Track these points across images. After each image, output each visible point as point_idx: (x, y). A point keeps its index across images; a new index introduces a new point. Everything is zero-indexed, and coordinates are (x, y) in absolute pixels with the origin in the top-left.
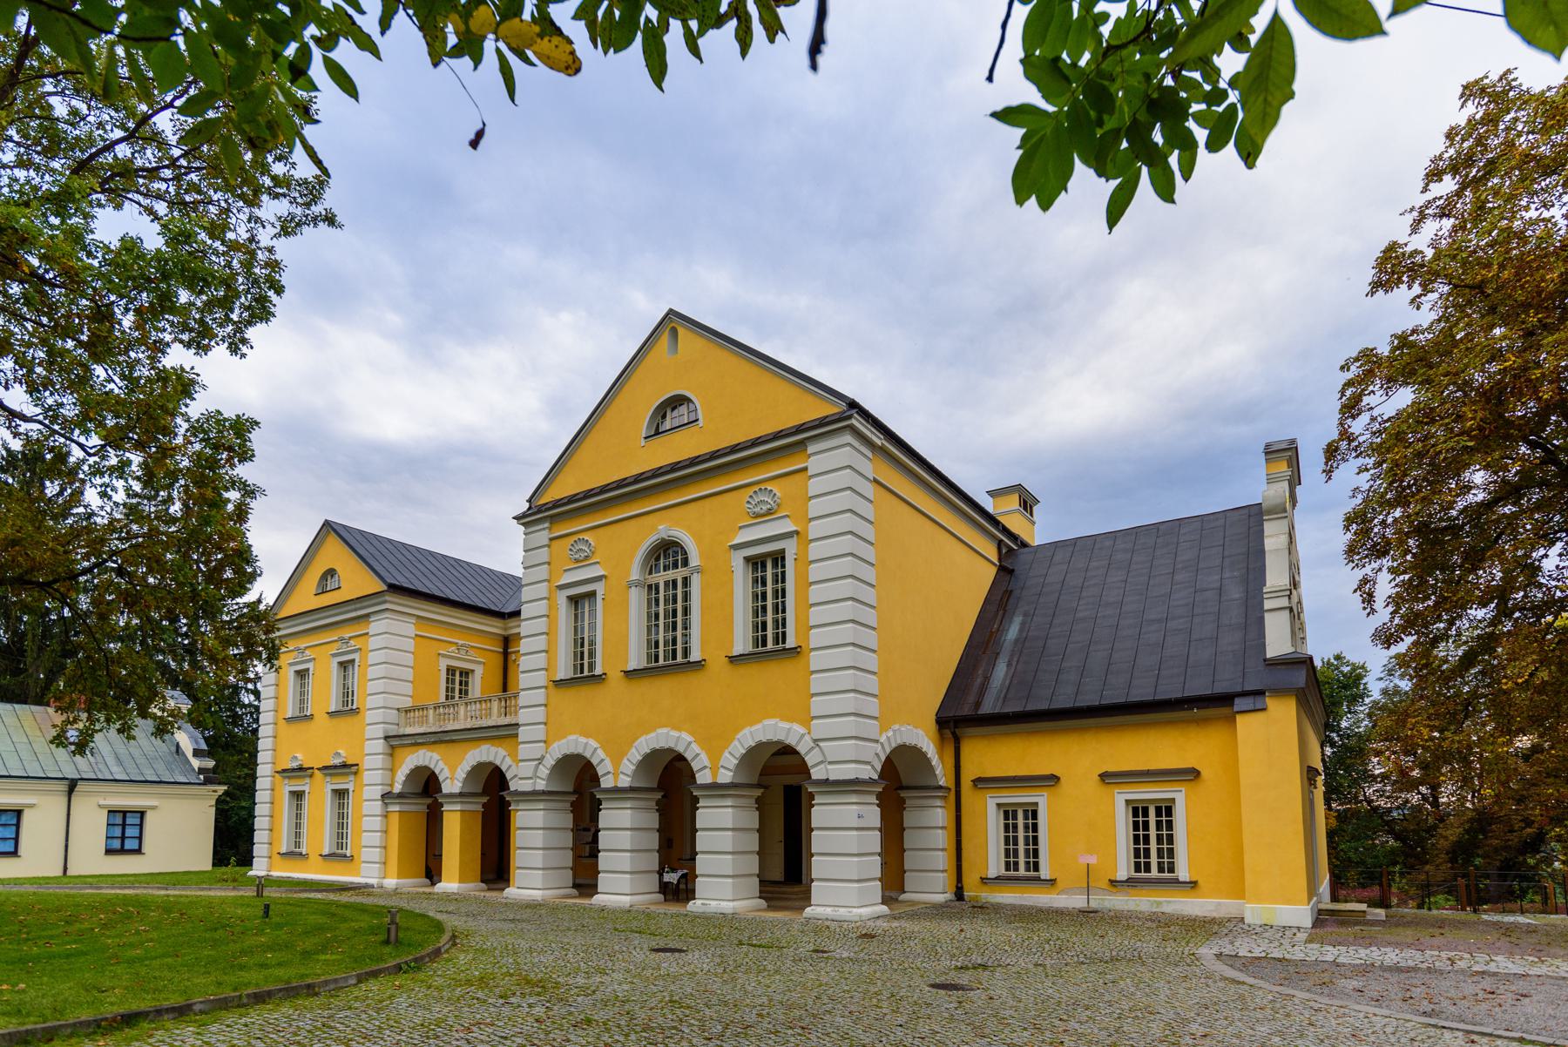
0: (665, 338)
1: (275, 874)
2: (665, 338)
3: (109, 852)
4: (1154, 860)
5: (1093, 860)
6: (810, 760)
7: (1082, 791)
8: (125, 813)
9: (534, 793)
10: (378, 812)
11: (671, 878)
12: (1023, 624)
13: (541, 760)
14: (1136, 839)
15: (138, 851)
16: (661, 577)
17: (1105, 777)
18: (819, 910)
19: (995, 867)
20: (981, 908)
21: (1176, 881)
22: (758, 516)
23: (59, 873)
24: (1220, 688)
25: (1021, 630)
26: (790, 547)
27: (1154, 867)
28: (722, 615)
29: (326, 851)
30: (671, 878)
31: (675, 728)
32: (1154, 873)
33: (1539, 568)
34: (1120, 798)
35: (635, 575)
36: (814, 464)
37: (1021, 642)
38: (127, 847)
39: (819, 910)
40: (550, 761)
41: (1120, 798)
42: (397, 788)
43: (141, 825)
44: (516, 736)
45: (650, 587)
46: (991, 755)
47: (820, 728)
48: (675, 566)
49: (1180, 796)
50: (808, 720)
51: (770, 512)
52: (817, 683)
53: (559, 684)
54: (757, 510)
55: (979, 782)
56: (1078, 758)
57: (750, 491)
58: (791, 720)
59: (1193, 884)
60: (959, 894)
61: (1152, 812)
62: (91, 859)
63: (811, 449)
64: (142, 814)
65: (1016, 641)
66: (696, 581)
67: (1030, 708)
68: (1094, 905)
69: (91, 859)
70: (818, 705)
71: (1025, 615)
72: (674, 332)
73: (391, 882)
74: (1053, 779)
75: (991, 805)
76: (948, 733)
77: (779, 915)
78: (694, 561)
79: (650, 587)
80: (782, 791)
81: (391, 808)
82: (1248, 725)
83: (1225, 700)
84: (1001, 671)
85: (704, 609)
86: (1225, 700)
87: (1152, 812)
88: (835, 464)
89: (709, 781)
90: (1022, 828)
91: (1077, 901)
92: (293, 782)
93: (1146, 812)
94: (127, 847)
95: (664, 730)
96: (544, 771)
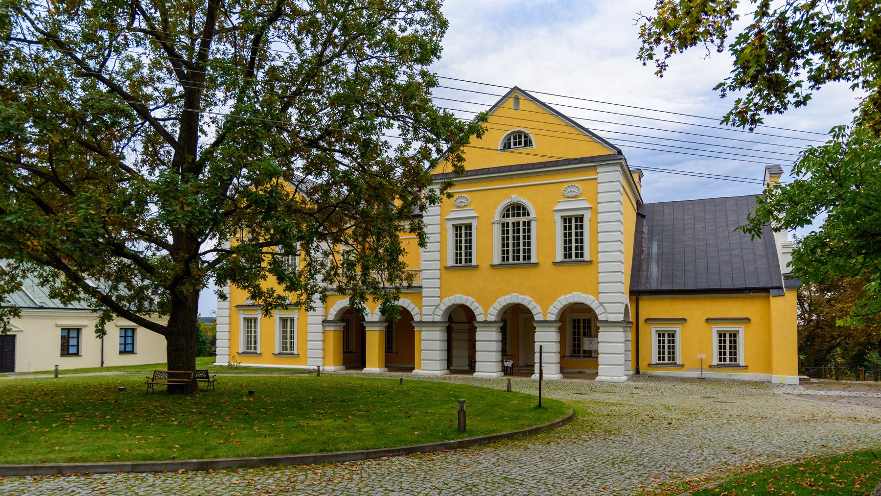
0: (510, 102)
1: (242, 365)
2: (510, 102)
3: (121, 353)
4: (728, 357)
5: (704, 356)
6: (597, 311)
7: (697, 327)
8: (69, 329)
9: (433, 322)
10: (227, 330)
11: (509, 364)
12: (659, 245)
13: (437, 306)
14: (735, 348)
15: (77, 354)
16: (510, 220)
17: (708, 320)
18: (603, 378)
19: (655, 360)
20: (652, 378)
21: (739, 366)
22: (569, 197)
23: (99, 365)
24: (762, 284)
25: (659, 248)
26: (587, 216)
27: (728, 359)
28: (547, 242)
29: (277, 352)
30: (509, 364)
31: (521, 293)
32: (728, 362)
33: (743, 64)
34: (715, 329)
35: (497, 217)
36: (601, 177)
37: (660, 255)
38: (71, 352)
39: (603, 378)
40: (443, 307)
41: (715, 329)
42: (331, 317)
43: (78, 338)
44: (421, 293)
45: (503, 224)
46: (651, 308)
47: (603, 298)
48: (519, 215)
49: (741, 329)
50: (597, 294)
51: (576, 196)
52: (602, 277)
53: (447, 268)
54: (570, 194)
55: (648, 320)
56: (695, 311)
57: (566, 185)
58: (587, 293)
59: (746, 367)
60: (637, 371)
61: (728, 336)
62: (114, 358)
63: (599, 170)
64: (78, 330)
65: (658, 254)
66: (534, 226)
67: (675, 288)
68: (704, 376)
69: (114, 358)
70: (602, 287)
71: (659, 241)
72: (517, 99)
73: (330, 368)
74: (684, 320)
75: (653, 331)
76: (634, 297)
77: (568, 381)
78: (533, 215)
79: (503, 224)
80: (579, 326)
81: (327, 329)
82: (775, 302)
83: (765, 290)
84: (654, 269)
85: (538, 239)
86: (765, 290)
87: (728, 336)
88: (609, 179)
89: (542, 319)
90: (666, 343)
91: (696, 374)
92: (247, 312)
93: (725, 336)
94: (71, 352)
95: (516, 294)
96: (440, 312)
